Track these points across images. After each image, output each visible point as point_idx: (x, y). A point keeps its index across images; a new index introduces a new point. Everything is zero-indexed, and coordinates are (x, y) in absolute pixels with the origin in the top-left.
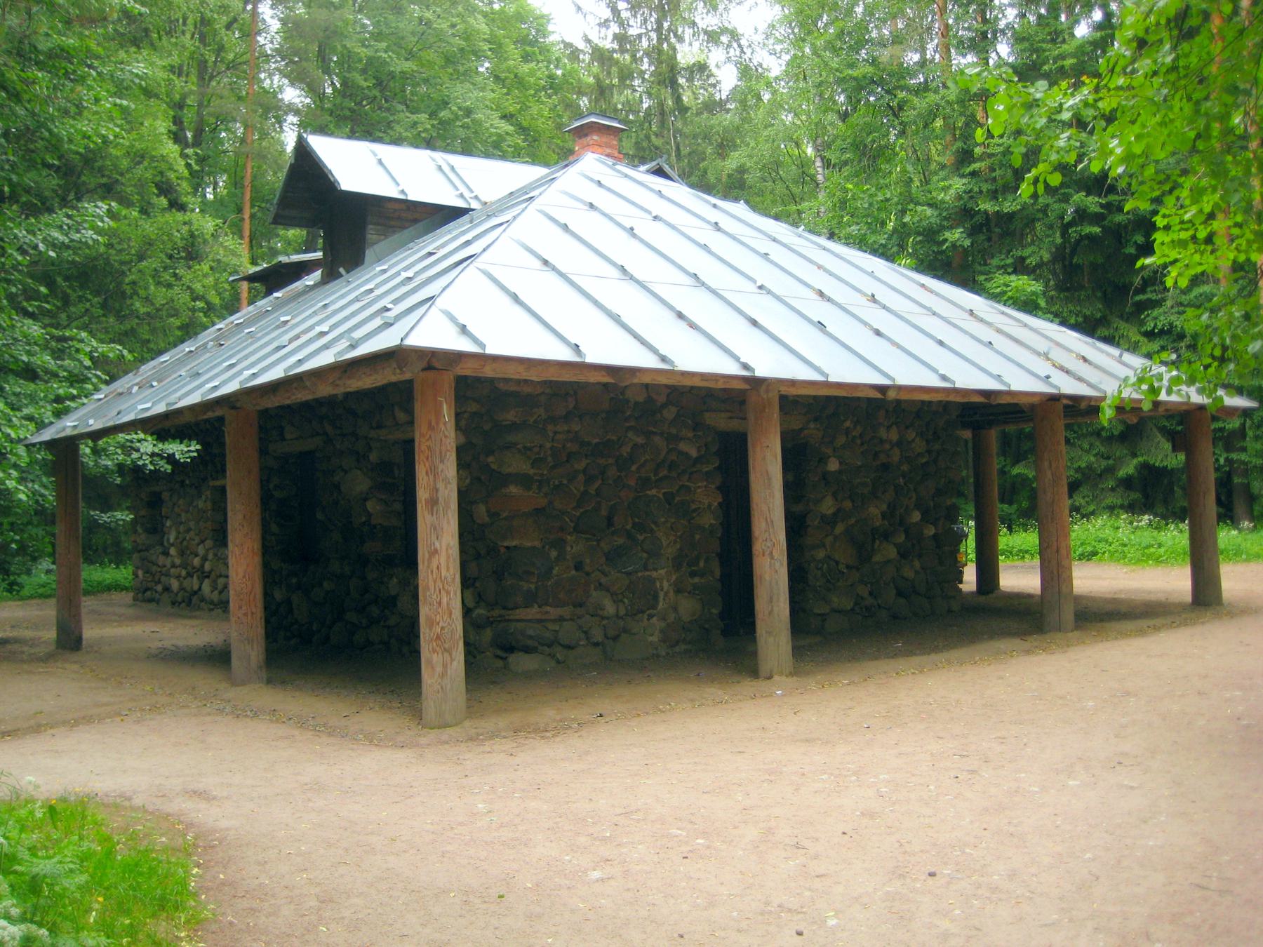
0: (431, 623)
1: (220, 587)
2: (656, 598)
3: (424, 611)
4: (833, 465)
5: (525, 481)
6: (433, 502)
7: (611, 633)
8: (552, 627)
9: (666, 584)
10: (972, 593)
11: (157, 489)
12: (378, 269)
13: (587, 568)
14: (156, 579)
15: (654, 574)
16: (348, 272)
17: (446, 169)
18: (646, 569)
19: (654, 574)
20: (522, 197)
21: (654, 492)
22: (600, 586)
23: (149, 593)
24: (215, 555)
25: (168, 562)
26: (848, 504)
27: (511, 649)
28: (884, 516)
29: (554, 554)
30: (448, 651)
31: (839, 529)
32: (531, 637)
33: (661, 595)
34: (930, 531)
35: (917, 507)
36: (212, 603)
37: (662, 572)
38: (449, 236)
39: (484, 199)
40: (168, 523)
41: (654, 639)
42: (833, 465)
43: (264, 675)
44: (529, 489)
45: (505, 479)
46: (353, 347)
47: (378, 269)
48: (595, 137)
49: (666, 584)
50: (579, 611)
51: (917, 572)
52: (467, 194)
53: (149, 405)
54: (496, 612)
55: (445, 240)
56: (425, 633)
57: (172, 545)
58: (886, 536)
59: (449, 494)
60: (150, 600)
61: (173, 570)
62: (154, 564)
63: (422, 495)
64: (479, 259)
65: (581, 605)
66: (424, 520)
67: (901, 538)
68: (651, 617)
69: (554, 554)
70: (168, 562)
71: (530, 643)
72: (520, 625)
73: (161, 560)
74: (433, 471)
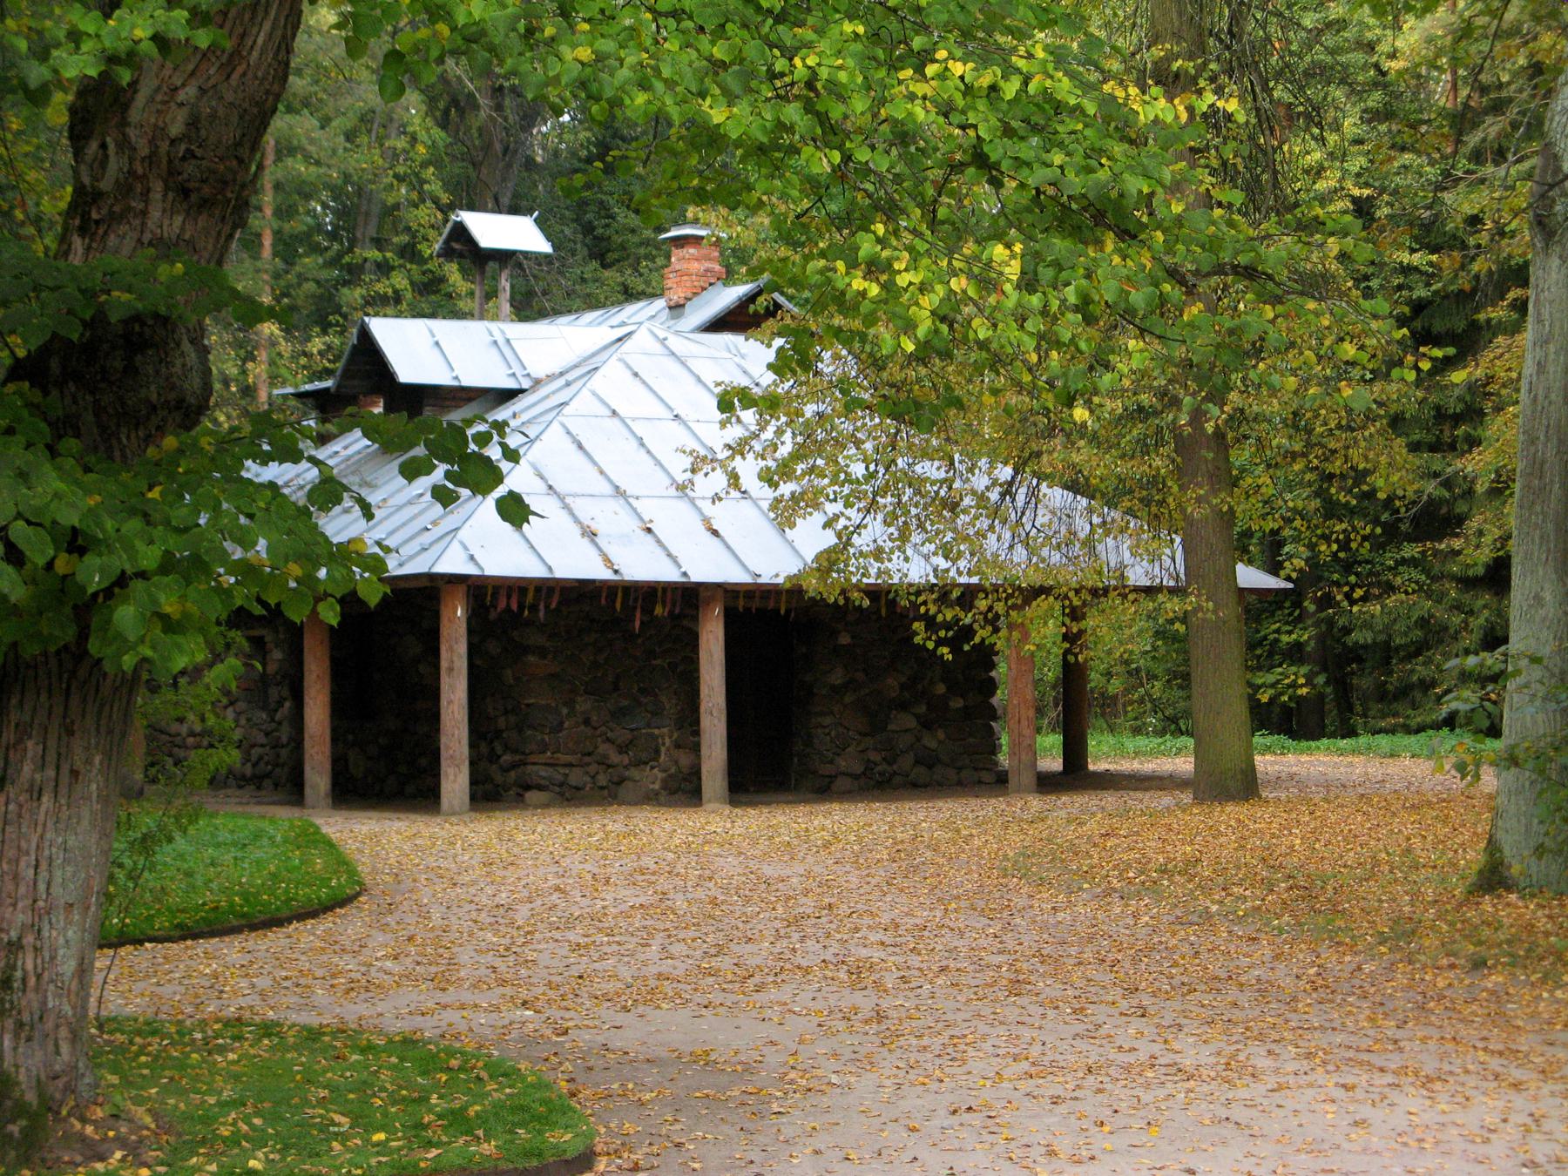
0: (448, 748)
1: (254, 758)
2: (657, 752)
3: (443, 740)
4: (844, 639)
5: (542, 652)
6: (451, 669)
7: (615, 779)
8: (562, 770)
9: (667, 741)
10: (1060, 773)
15: (656, 732)
17: (501, 342)
18: (649, 726)
19: (656, 732)
20: (588, 366)
21: (658, 662)
22: (608, 740)
24: (248, 720)
25: (184, 730)
26: (860, 676)
27: (528, 788)
28: (903, 687)
31: (848, 699)
33: (663, 749)
34: (957, 703)
35: (943, 680)
36: (243, 777)
37: (665, 730)
39: (534, 375)
41: (657, 786)
42: (844, 639)
43: (330, 801)
44: (545, 657)
45: (526, 650)
46: (401, 565)
48: (692, 251)
49: (667, 741)
50: (587, 759)
51: (940, 742)
54: (517, 758)
56: (444, 754)
58: (903, 706)
59: (462, 664)
62: (162, 732)
63: (444, 664)
65: (589, 754)
67: (922, 709)
71: (543, 782)
72: (535, 768)
74: (451, 649)
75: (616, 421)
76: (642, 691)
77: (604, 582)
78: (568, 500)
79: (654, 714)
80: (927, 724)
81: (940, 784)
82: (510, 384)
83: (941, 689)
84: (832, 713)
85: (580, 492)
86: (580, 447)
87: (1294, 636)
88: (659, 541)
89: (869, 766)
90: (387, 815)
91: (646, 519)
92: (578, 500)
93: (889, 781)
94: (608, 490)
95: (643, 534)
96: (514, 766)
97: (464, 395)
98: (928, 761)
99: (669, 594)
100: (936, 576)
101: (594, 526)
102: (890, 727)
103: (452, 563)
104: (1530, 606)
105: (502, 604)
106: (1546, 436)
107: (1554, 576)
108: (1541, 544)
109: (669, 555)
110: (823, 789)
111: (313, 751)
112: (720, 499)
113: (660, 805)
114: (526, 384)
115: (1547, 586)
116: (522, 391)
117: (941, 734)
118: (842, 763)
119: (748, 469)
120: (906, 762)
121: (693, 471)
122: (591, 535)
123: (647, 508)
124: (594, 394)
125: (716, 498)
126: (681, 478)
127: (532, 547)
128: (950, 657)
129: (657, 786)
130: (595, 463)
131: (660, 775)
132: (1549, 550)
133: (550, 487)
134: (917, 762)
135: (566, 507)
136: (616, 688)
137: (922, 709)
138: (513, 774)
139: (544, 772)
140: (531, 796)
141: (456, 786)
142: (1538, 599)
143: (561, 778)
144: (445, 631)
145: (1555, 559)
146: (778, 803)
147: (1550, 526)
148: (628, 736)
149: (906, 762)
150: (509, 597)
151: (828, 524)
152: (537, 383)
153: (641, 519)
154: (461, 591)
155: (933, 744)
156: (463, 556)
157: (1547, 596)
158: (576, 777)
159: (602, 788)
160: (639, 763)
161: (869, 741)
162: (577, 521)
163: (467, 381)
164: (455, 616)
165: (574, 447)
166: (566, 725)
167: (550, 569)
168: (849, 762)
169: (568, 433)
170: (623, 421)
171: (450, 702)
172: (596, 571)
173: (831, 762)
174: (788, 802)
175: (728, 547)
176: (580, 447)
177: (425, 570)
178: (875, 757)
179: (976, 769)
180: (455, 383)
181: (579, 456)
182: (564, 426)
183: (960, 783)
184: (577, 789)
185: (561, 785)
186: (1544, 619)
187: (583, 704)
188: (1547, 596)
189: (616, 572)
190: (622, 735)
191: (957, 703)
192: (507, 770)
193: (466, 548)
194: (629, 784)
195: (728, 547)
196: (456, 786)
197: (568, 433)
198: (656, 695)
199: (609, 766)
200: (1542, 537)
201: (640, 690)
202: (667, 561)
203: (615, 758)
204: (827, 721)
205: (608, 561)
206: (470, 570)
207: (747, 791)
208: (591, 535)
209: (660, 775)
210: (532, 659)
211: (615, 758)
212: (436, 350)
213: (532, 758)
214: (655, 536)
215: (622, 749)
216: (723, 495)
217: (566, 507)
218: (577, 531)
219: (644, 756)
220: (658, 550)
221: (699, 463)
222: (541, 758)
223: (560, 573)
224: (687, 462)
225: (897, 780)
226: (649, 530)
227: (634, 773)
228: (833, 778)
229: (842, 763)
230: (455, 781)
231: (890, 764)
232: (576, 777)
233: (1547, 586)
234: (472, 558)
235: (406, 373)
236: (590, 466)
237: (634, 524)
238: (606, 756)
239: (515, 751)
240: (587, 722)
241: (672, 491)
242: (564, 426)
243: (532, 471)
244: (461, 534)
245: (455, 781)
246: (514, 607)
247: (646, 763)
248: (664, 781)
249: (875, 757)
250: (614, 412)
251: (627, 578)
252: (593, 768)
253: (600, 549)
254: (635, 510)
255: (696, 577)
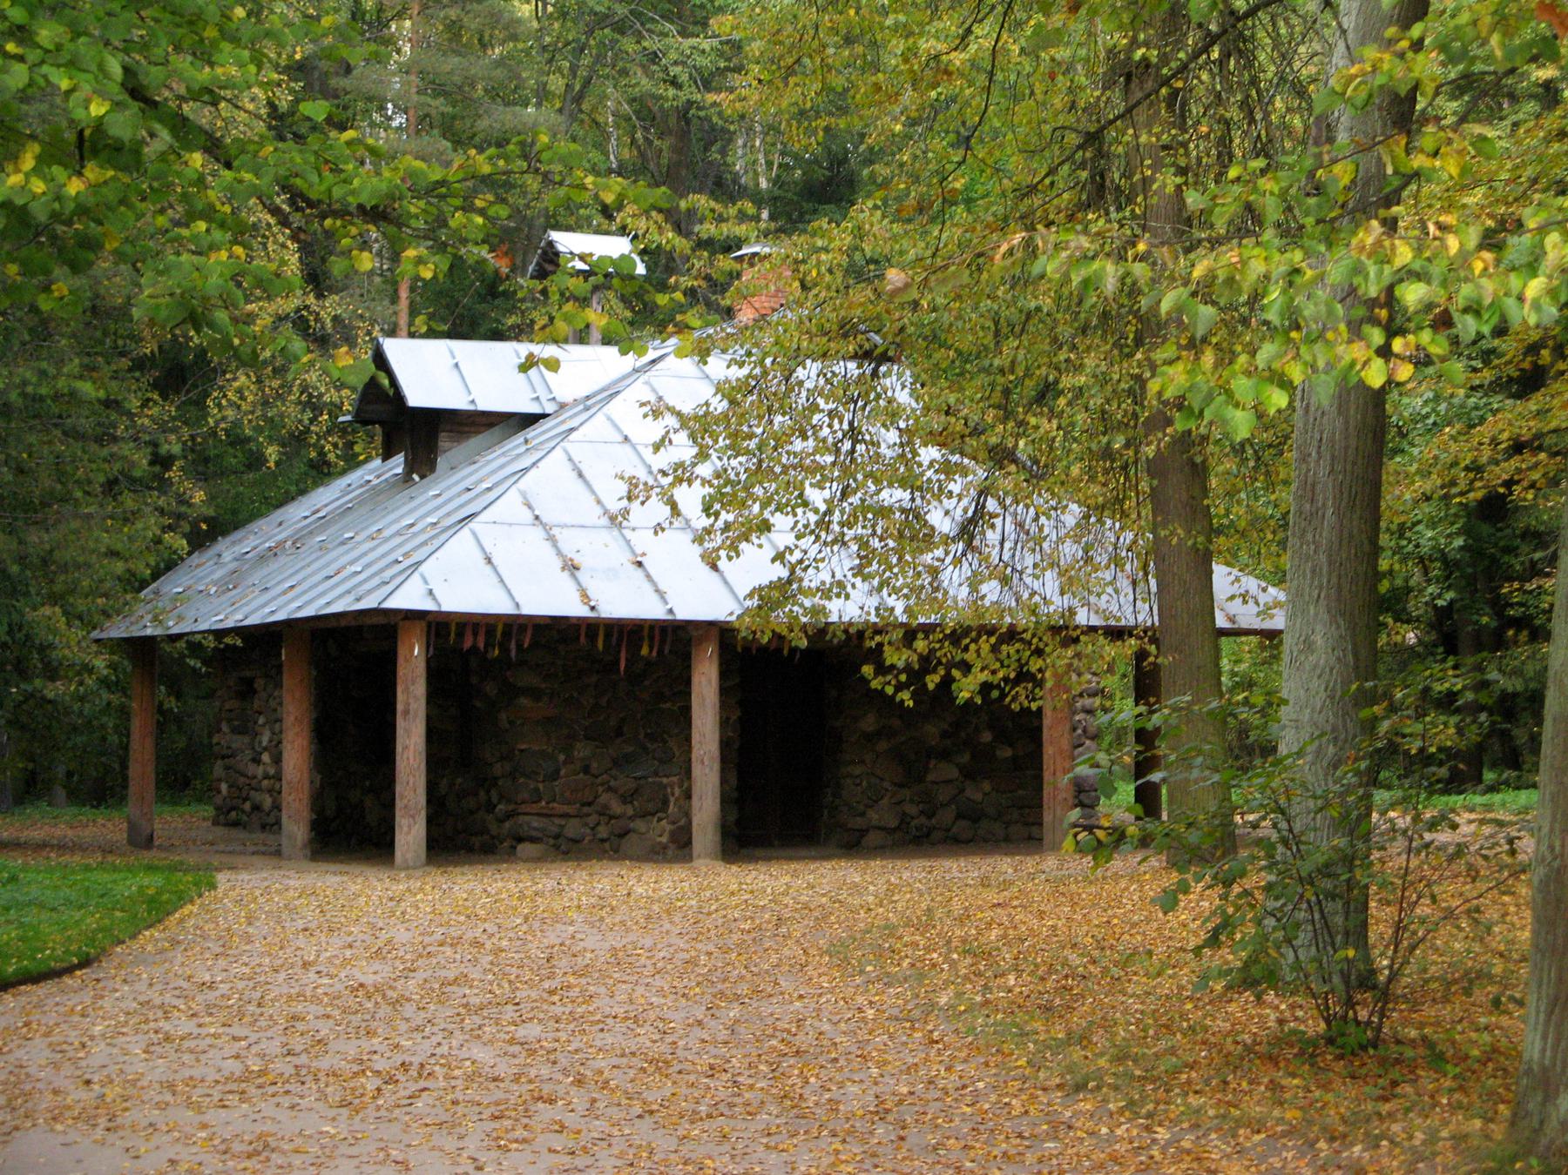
2: (666, 802)
3: (398, 789)
5: (536, 694)
6: (406, 712)
8: (557, 821)
11: (248, 674)
12: (432, 493)
13: (594, 771)
14: (244, 794)
15: (665, 780)
16: (422, 477)
18: (656, 774)
21: (668, 705)
22: (610, 789)
23: (233, 814)
25: (260, 771)
27: (520, 840)
28: (945, 735)
29: (562, 757)
30: (413, 817)
32: (535, 829)
33: (672, 800)
37: (675, 779)
38: (502, 460)
39: (559, 399)
40: (261, 720)
41: (664, 839)
46: (358, 600)
47: (432, 493)
50: (586, 810)
52: (544, 396)
53: (221, 617)
54: (511, 807)
55: (534, 432)
56: (399, 804)
57: (265, 749)
58: (945, 755)
60: (235, 824)
61: (265, 782)
63: (400, 707)
64: (478, 519)
65: (589, 804)
66: (401, 724)
67: (965, 758)
68: (660, 820)
69: (562, 757)
70: (260, 771)
71: (534, 833)
72: (527, 818)
73: (252, 769)
75: (627, 447)
76: (651, 737)
77: (581, 620)
78: (555, 531)
79: (662, 762)
80: (969, 774)
81: (985, 841)
82: (535, 409)
83: (987, 737)
84: (862, 762)
85: (569, 521)
86: (580, 475)
87: (1447, 685)
88: (648, 576)
89: (904, 819)
90: (974, 854)
91: (639, 551)
92: (565, 531)
93: (928, 835)
94: (529, 517)
95: (634, 567)
96: (509, 815)
97: (484, 420)
98: (973, 815)
99: (657, 632)
100: (878, 615)
101: (578, 559)
102: (930, 777)
103: (409, 598)
104: (1301, 652)
105: (468, 643)
106: (1318, 453)
107: (1326, 617)
108: (1312, 578)
109: (657, 591)
110: (853, 845)
111: (291, 798)
112: (663, 530)
113: (670, 861)
114: (550, 408)
115: (1318, 628)
116: (544, 416)
117: (987, 786)
118: (874, 816)
119: (684, 495)
120: (946, 816)
121: (629, 498)
122: (572, 568)
123: (571, 542)
124: (609, 419)
125: (658, 529)
126: (615, 506)
127: (502, 581)
128: (911, 703)
129: (664, 839)
130: (593, 492)
131: (669, 828)
132: (1321, 588)
133: (537, 518)
134: (959, 816)
135: (552, 540)
136: (619, 733)
137: (965, 758)
138: (507, 825)
139: (536, 823)
140: (525, 848)
141: (410, 838)
142: (1309, 646)
143: (555, 830)
144: (402, 671)
145: (1328, 596)
146: (778, 858)
147: (1323, 558)
148: (632, 785)
149: (946, 816)
150: (475, 634)
151: (779, 557)
152: (563, 406)
153: (633, 552)
154: (419, 629)
155: (978, 797)
156: (423, 589)
157: (1319, 640)
158: (573, 828)
159: (603, 841)
160: (644, 815)
161: (906, 793)
162: (559, 553)
163: (483, 406)
164: (413, 657)
165: (574, 474)
166: (562, 772)
167: (517, 605)
168: (882, 815)
169: (570, 460)
170: (634, 447)
171: (406, 748)
172: (567, 605)
173: (863, 814)
174: (814, 859)
175: (726, 582)
176: (580, 475)
177: (375, 605)
178: (912, 810)
179: (1026, 824)
180: (471, 408)
181: (579, 484)
182: (567, 452)
183: (1007, 839)
184: (575, 841)
185: (557, 837)
186: (1315, 667)
187: (582, 751)
188: (1319, 640)
189: (593, 608)
190: (624, 783)
191: (1005, 753)
192: (502, 821)
193: (426, 582)
194: (633, 837)
195: (726, 582)
196: (410, 838)
197: (570, 460)
198: (665, 742)
199: (611, 817)
200: (1313, 571)
201: (647, 735)
202: (655, 597)
203: (617, 808)
204: (857, 770)
205: (585, 596)
206: (428, 606)
207: (771, 845)
208: (572, 568)
209: (669, 828)
210: (524, 701)
211: (617, 808)
212: (455, 372)
213: (523, 808)
214: (645, 570)
215: (626, 799)
216: (666, 525)
217: (552, 540)
218: (558, 563)
219: (650, 807)
220: (647, 586)
221: (635, 491)
222: (535, 808)
223: (528, 609)
224: (623, 488)
225: (936, 835)
226: (640, 564)
227: (639, 825)
228: (863, 832)
229: (874, 816)
230: (411, 832)
231: (929, 817)
232: (573, 828)
233: (1318, 628)
234: (431, 592)
235: (416, 397)
236: (587, 494)
237: (625, 557)
238: (606, 807)
239: (509, 801)
240: (586, 770)
241: (605, 521)
242: (567, 452)
243: (521, 499)
244: (423, 568)
245: (411, 832)
246: (481, 645)
247: (653, 815)
248: (672, 834)
249: (912, 810)
250: (626, 438)
251: (603, 615)
252: (592, 820)
253: (579, 584)
254: (628, 542)
255: (682, 614)
